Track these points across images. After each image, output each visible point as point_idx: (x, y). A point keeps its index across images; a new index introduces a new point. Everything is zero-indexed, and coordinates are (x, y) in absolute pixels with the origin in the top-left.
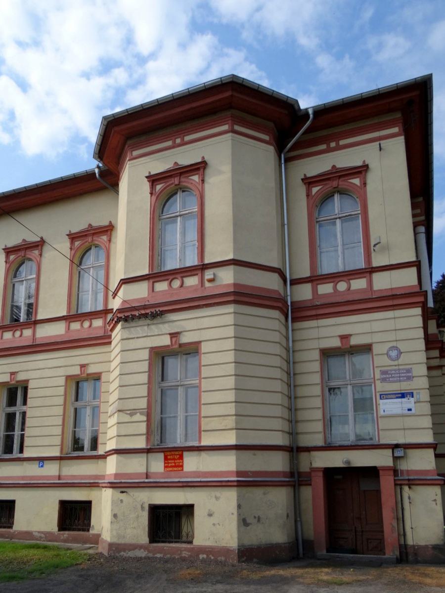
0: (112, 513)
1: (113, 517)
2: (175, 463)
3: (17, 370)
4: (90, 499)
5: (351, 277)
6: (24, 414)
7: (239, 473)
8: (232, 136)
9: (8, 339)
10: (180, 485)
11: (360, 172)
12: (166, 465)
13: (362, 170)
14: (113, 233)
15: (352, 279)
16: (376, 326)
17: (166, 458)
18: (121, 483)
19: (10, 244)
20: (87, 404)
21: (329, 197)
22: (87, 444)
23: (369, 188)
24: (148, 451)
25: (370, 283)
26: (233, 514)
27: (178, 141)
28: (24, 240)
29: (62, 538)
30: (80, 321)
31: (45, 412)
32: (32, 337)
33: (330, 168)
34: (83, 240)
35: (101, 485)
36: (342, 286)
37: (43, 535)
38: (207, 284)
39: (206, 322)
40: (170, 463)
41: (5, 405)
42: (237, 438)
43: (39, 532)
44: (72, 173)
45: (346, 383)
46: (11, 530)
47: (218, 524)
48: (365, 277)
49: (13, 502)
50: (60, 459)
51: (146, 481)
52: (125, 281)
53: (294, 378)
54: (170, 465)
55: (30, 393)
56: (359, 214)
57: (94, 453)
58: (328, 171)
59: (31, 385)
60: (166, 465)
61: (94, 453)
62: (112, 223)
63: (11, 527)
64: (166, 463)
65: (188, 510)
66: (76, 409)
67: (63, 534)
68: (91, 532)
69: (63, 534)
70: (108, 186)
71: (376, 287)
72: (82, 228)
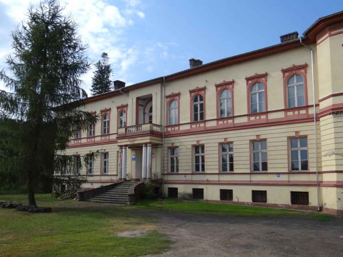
0: (337, 198)
1: (338, 199)
3: (299, 130)
4: (308, 191)
5: (261, 115)
6: (203, 157)
7: (337, 182)
9: (252, 120)
14: (111, 111)
15: (228, 120)
16: (203, 138)
19: (218, 83)
20: (259, 151)
21: (292, 76)
22: (261, 167)
28: (256, 74)
29: (294, 207)
30: (293, 111)
31: (211, 156)
32: (266, 119)
33: (196, 87)
34: (290, 72)
35: (321, 185)
36: (296, 113)
37: (284, 206)
41: (104, 158)
42: (336, 168)
43: (281, 204)
44: (223, 58)
46: (266, 203)
48: (265, 115)
49: (266, 192)
50: (100, 175)
51: (288, 183)
55: (205, 149)
58: (253, 76)
59: (205, 146)
61: (105, 173)
62: (267, 72)
63: (266, 202)
66: (254, 154)
67: (295, 206)
68: (309, 205)
69: (295, 206)
70: (304, 45)
71: (96, 140)
72: (290, 67)
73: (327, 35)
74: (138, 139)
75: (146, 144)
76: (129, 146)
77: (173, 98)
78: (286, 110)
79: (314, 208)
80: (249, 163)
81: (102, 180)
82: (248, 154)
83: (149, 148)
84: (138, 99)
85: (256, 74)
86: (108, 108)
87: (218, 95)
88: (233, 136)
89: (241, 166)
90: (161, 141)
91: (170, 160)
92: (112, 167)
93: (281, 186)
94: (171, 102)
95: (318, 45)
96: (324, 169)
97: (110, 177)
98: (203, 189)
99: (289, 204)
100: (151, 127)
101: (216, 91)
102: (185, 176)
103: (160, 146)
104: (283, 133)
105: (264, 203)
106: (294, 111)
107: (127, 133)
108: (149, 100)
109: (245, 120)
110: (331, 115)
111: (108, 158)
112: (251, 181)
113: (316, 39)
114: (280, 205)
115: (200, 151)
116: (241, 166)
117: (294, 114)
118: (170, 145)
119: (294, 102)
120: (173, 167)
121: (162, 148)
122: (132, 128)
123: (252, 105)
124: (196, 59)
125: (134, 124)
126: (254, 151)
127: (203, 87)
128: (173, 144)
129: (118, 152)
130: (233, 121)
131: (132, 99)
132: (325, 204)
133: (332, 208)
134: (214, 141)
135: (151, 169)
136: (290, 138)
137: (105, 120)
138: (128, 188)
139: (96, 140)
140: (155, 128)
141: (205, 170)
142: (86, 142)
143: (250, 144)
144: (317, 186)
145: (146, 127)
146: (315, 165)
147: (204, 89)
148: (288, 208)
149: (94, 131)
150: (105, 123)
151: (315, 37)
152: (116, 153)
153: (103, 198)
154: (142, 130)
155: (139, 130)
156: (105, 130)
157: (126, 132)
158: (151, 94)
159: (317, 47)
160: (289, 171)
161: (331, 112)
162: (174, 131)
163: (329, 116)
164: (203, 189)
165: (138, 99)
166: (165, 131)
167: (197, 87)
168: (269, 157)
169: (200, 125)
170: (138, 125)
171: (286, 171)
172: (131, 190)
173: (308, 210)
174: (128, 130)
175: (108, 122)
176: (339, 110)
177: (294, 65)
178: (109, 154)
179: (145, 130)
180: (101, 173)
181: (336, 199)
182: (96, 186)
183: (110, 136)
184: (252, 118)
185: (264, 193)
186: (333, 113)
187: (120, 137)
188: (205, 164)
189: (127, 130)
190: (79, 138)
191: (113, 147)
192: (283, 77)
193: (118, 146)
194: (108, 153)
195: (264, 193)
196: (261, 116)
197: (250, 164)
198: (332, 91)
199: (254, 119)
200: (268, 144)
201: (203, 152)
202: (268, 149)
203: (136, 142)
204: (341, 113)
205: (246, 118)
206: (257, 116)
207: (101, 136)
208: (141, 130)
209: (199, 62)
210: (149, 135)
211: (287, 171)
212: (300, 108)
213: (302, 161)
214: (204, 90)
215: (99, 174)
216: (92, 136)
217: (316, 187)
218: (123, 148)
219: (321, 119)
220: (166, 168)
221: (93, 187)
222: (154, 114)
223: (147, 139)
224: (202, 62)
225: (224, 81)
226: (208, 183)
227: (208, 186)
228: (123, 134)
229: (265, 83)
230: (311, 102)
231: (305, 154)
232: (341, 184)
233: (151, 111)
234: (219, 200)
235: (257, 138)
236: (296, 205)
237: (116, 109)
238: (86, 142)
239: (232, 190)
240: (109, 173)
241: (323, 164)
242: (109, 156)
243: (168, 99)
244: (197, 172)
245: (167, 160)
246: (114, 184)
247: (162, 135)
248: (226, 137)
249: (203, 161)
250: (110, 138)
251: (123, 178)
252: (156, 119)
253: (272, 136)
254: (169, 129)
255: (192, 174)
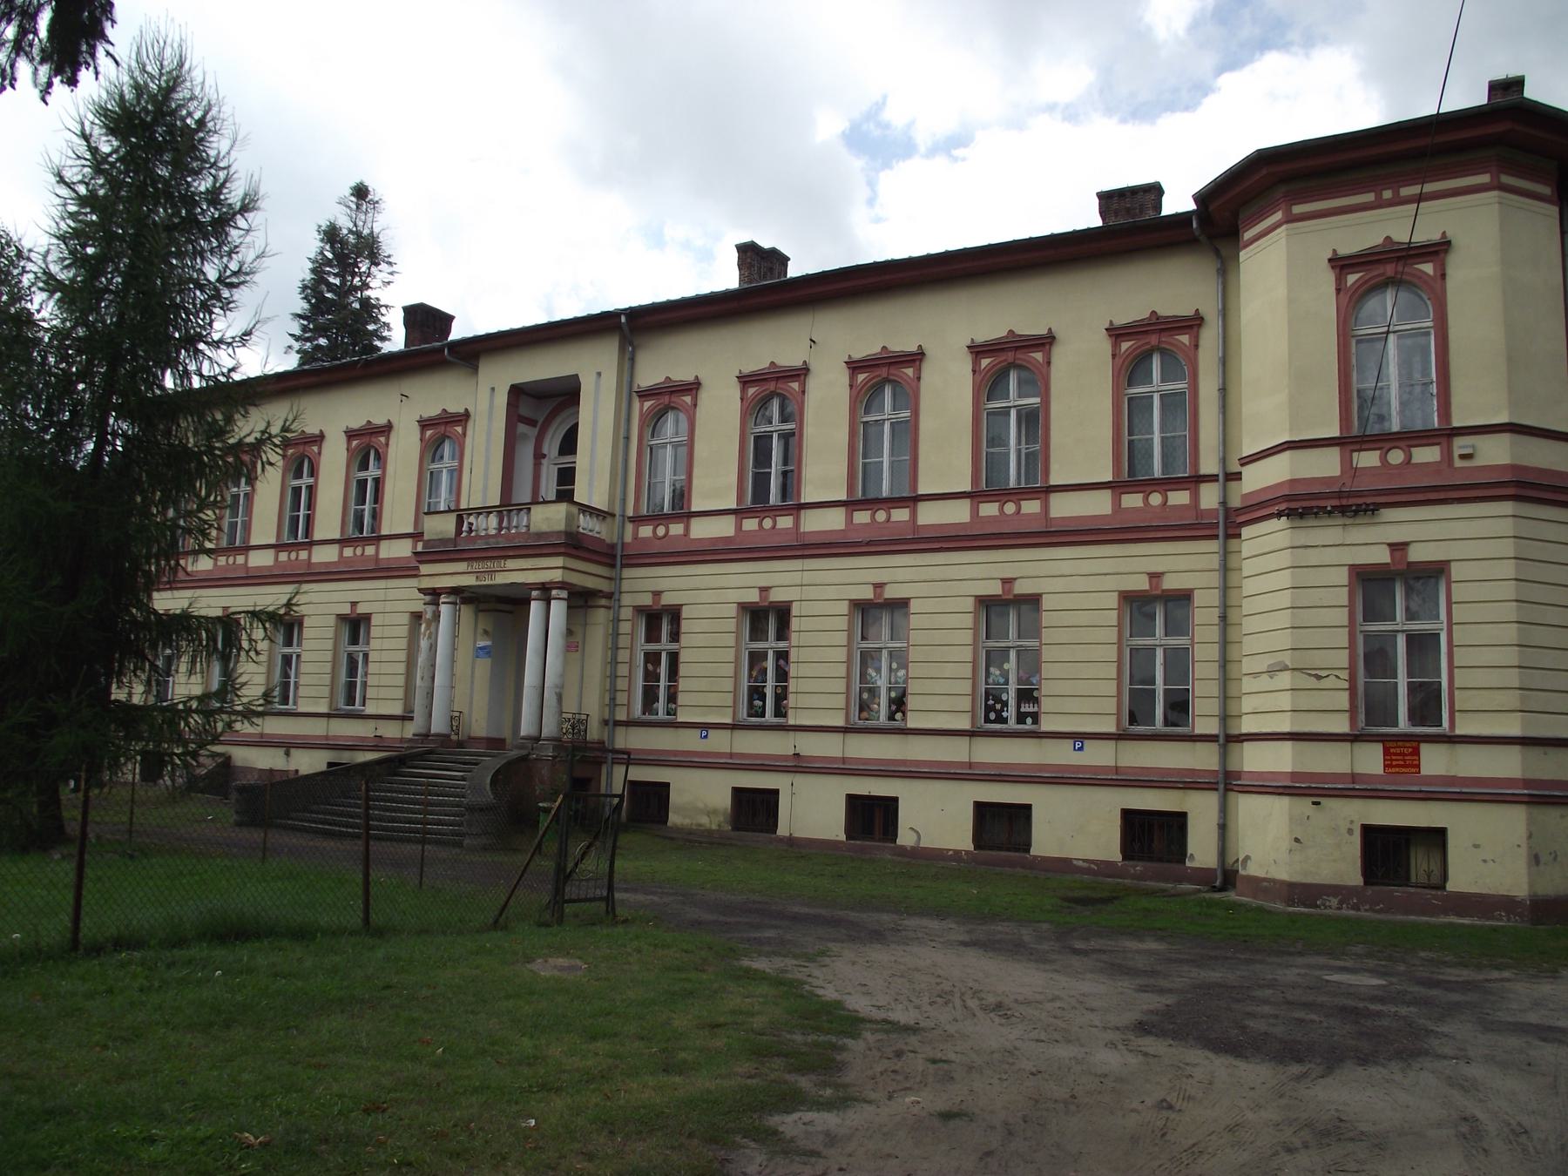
2: (1404, 760)
6: (674, 658)
7: (1294, 775)
8: (1499, 197)
10: (1420, 795)
11: (1190, 327)
12: (1386, 763)
13: (1438, 250)
15: (981, 502)
16: (1029, 569)
17: (1386, 752)
18: (1310, 788)
23: (1452, 284)
24: (1353, 738)
25: (1046, 507)
26: (1519, 846)
27: (1387, 194)
29: (1132, 871)
38: (1458, 463)
39: (1460, 529)
40: (1401, 760)
43: (1084, 860)
45: (1395, 628)
47: (1493, 860)
50: (328, 716)
51: (1351, 786)
52: (1292, 445)
53: (620, 583)
54: (1394, 763)
55: (795, 624)
56: (1431, 327)
57: (648, 717)
59: (795, 611)
60: (1386, 763)
63: (1028, 851)
64: (1388, 760)
65: (1436, 837)
71: (893, 519)
73: (1278, 216)
74: (511, 564)
75: (545, 590)
76: (466, 595)
77: (445, 431)
78: (975, 496)
79: (1203, 876)
80: (969, 691)
81: (335, 738)
82: (967, 654)
83: (558, 609)
84: (516, 392)
85: (1011, 332)
86: (380, 420)
87: (855, 402)
88: (908, 578)
89: (1071, 705)
90: (607, 581)
91: (640, 659)
92: (385, 680)
93: (1513, 805)
94: (658, 416)
95: (1246, 246)
96: (1248, 726)
97: (372, 724)
98: (666, 786)
99: (840, 838)
100: (570, 518)
101: (851, 386)
102: (704, 733)
103: (603, 602)
104: (1103, 577)
105: (1017, 854)
106: (876, 511)
107: (464, 534)
108: (561, 399)
109: (958, 513)
110: (1284, 519)
111: (368, 644)
112: (970, 765)
113: (1237, 226)
114: (1080, 863)
115: (665, 628)
116: (1071, 705)
117: (875, 520)
118: (647, 600)
119: (1151, 456)
120: (650, 696)
121: (608, 608)
122: (477, 518)
123: (1131, 442)
124: (765, 244)
125: (495, 500)
126: (991, 644)
127: (798, 363)
128: (657, 594)
129: (417, 617)
130: (914, 514)
131: (489, 390)
132: (1247, 858)
133: (1269, 876)
134: (831, 592)
135: (560, 697)
136: (1130, 600)
137: (362, 475)
138: (463, 779)
139: (314, 560)
140: (586, 524)
141: (790, 713)
142: (335, 559)
143: (976, 613)
144: (1216, 789)
145: (549, 518)
146: (1213, 707)
147: (801, 373)
148: (1109, 877)
149: (309, 520)
150: (362, 484)
151: (1236, 215)
152: (405, 619)
153: (341, 814)
154: (533, 529)
155: (508, 529)
156: (295, 521)
157: (459, 531)
158: (576, 376)
159: (1242, 254)
160: (1118, 729)
161: (1283, 507)
162: (667, 538)
163: (1275, 521)
164: (776, 792)
165: (516, 392)
166: (628, 538)
167: (772, 363)
168: (1046, 670)
169: (364, 550)
170: (507, 506)
171: (1110, 727)
172: (478, 783)
173: (1180, 882)
174: (471, 524)
175: (378, 482)
176: (1314, 503)
177: (1154, 313)
178: (373, 622)
179: (545, 528)
180: (405, 704)
181: (1286, 844)
182: (308, 763)
183: (316, 549)
184: (989, 509)
185: (1022, 813)
186: (1290, 514)
187: (437, 552)
188: (792, 685)
189: (465, 524)
190: (237, 544)
191: (392, 594)
192: (1114, 356)
193: (420, 590)
194: (367, 618)
195: (1022, 813)
196: (1023, 503)
197: (974, 694)
198: (1291, 430)
199: (1140, 504)
200: (1046, 618)
201: (675, 636)
202: (1047, 636)
203: (501, 579)
204: (1356, 513)
205: (335, 549)
206: (1155, 491)
207: (343, 542)
208: (528, 526)
209: (776, 259)
210: (562, 550)
211: (964, 723)
212: (1168, 484)
213: (1166, 691)
214: (694, 392)
215: (323, 708)
216: (300, 539)
217: (1215, 792)
218: (443, 599)
219: (1246, 532)
220: (621, 698)
221: (292, 767)
222: (581, 460)
223: (550, 570)
224: (450, 319)
225: (884, 348)
226: (799, 765)
227: (800, 780)
228: (443, 541)
229: (800, 401)
230: (1209, 464)
231: (1179, 662)
232: (1261, 784)
233: (569, 444)
234: (843, 837)
235: (875, 596)
236: (1140, 863)
237: (343, 438)
238: (335, 559)
239: (896, 800)
240: (370, 709)
241: (1247, 704)
242: (374, 632)
243: (647, 404)
244: (648, 717)
245: (631, 663)
246: (396, 757)
247: (614, 556)
248: (1160, 569)
249: (782, 675)
250: (383, 554)
251: (546, 733)
252: (590, 484)
253: (1058, 585)
254: (646, 531)
255: (734, 727)
